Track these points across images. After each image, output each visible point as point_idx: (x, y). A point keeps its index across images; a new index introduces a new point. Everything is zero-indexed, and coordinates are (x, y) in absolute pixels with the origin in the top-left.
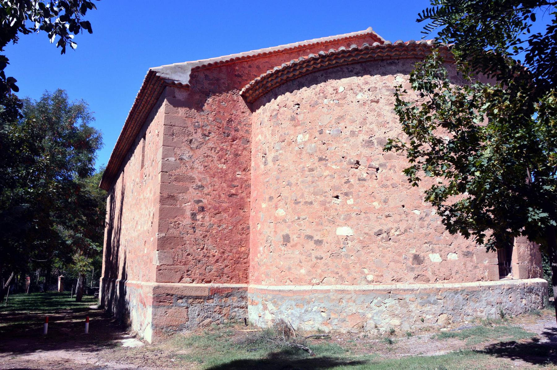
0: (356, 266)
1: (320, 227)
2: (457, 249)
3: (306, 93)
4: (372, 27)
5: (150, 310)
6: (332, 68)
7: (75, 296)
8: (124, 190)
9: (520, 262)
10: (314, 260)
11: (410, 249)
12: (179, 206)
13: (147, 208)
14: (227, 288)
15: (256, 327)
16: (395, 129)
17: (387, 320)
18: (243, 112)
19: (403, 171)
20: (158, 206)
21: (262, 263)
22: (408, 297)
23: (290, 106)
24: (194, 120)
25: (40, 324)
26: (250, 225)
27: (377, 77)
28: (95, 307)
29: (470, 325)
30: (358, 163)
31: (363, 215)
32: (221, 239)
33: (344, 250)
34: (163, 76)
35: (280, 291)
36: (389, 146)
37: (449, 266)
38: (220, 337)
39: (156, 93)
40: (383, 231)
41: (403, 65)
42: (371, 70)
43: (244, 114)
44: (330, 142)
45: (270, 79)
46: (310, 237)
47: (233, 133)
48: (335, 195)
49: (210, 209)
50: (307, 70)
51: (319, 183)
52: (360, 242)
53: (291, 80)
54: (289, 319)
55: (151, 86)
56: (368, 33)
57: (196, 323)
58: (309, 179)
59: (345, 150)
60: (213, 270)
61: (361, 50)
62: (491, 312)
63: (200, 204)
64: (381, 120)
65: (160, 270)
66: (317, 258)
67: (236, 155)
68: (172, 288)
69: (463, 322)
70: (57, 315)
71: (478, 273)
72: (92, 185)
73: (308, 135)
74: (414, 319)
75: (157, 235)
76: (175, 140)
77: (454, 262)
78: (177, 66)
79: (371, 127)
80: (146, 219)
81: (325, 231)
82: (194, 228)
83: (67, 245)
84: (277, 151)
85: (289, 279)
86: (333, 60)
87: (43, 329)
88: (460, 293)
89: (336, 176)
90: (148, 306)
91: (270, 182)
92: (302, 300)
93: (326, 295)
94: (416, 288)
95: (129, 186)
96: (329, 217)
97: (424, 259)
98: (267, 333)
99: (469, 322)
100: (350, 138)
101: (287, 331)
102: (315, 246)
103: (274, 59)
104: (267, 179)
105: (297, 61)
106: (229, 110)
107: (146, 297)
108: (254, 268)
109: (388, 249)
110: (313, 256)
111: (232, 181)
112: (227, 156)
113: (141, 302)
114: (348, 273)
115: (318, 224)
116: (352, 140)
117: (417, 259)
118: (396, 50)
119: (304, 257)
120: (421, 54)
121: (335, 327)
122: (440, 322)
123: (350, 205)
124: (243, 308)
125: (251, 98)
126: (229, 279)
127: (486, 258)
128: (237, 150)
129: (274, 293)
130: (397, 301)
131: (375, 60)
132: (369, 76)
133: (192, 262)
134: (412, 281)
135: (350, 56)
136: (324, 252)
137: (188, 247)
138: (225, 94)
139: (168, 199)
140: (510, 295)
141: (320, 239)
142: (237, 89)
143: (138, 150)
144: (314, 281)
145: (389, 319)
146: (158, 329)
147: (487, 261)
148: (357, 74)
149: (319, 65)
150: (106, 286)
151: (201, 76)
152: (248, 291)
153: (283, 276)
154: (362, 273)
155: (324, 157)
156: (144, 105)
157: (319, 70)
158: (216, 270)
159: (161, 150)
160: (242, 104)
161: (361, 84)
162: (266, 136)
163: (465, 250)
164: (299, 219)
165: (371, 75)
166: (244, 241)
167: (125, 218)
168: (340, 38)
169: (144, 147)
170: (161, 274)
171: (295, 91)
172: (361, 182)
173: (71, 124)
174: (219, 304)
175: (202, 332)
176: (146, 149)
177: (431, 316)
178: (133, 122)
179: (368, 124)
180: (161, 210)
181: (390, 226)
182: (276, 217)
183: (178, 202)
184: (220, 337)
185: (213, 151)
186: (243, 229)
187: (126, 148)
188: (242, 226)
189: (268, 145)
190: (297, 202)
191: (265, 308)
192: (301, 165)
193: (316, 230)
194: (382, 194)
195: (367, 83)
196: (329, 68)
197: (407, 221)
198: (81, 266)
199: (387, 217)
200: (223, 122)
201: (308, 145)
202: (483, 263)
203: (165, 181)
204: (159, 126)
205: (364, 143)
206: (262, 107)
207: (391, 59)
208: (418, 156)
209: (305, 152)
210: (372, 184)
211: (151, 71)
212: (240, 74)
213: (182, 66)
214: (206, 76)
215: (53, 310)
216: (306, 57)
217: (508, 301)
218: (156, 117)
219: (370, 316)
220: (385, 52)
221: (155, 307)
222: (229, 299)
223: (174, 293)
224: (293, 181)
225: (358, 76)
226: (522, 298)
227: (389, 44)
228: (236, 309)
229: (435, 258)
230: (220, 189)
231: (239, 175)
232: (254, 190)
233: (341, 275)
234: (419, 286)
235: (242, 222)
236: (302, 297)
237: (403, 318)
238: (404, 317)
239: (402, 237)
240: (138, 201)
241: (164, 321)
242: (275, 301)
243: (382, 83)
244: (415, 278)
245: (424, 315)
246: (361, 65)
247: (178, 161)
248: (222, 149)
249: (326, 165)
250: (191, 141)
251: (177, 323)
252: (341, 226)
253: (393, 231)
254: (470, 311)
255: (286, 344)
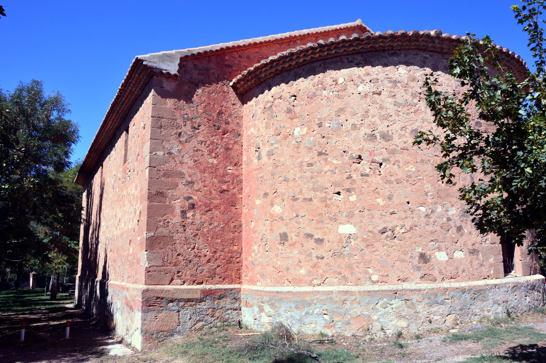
0: (359, 266)
1: (320, 225)
2: (463, 247)
3: (303, 85)
4: (362, 19)
5: (138, 315)
6: (332, 58)
7: (49, 293)
8: (104, 184)
9: (523, 258)
10: (315, 260)
11: (416, 247)
12: (168, 203)
13: (132, 205)
14: (219, 289)
15: (252, 331)
16: (398, 122)
17: (393, 322)
18: (234, 104)
19: (436, 167)
20: (146, 203)
21: (257, 263)
22: (415, 298)
23: (286, 98)
24: (182, 112)
25: (16, 328)
26: (243, 223)
27: (379, 68)
28: (71, 306)
29: (479, 326)
30: (360, 157)
31: (366, 212)
32: (212, 238)
33: (347, 248)
34: (150, 64)
35: (278, 292)
36: (420, 139)
37: (455, 264)
38: (216, 343)
39: (141, 83)
40: (388, 229)
41: (406, 56)
42: (372, 60)
43: (235, 107)
44: (330, 136)
45: (264, 69)
46: (310, 236)
47: (224, 126)
48: (337, 191)
49: (200, 206)
50: (304, 60)
51: (318, 179)
52: (364, 240)
53: (286, 70)
54: (289, 322)
55: (137, 75)
56: (358, 25)
57: (188, 327)
58: (308, 174)
59: (346, 144)
60: (205, 271)
61: (363, 40)
62: (497, 311)
63: (191, 201)
64: (383, 112)
65: (149, 272)
66: (318, 257)
67: (227, 149)
68: (162, 291)
69: (471, 322)
70: (32, 317)
71: (485, 271)
72: (68, 178)
73: (306, 129)
74: (422, 321)
75: (145, 235)
76: (163, 133)
77: (460, 261)
78: (165, 54)
79: (373, 120)
80: (131, 216)
81: (326, 229)
82: (184, 226)
83: (44, 243)
84: (272, 145)
85: (287, 279)
86: (333, 50)
87: (19, 334)
88: (468, 292)
89: (337, 171)
90: (135, 310)
91: (265, 178)
92: (302, 302)
93: (329, 296)
94: (423, 288)
95: (109, 182)
96: (330, 214)
97: (430, 258)
98: (265, 336)
99: (477, 322)
100: (352, 132)
101: (288, 336)
102: (316, 244)
103: (264, 50)
104: (262, 175)
105: (294, 50)
106: (220, 102)
107: (134, 301)
108: (247, 267)
109: (394, 247)
110: (314, 255)
111: (224, 176)
112: (218, 150)
113: (127, 305)
114: (352, 273)
115: (318, 222)
116: (354, 133)
117: (422, 256)
118: (399, 40)
119: (304, 257)
120: (424, 45)
121: (339, 331)
122: (448, 323)
123: (352, 202)
124: (236, 310)
125: (242, 89)
126: (221, 280)
127: (492, 256)
128: (228, 143)
129: (272, 294)
130: (404, 302)
131: (377, 51)
132: (370, 67)
133: (183, 263)
134: (418, 280)
135: (351, 45)
136: (326, 251)
137: (178, 246)
138: (214, 85)
139: (156, 196)
140: (515, 293)
141: (321, 238)
142: (228, 80)
143: (120, 144)
144: (315, 282)
145: (396, 321)
146: (148, 335)
147: (492, 259)
148: (358, 65)
149: (318, 55)
150: (84, 284)
151: (190, 65)
152: (242, 292)
153: (280, 277)
154: (367, 273)
155: (324, 152)
156: (128, 96)
157: (317, 60)
158: (208, 270)
159: (148, 144)
160: (233, 96)
161: (362, 76)
162: (259, 130)
163: (471, 247)
164: (297, 216)
165: (373, 66)
166: (236, 240)
167: (105, 215)
168: (330, 30)
169: (126, 141)
170: (149, 276)
171: (291, 82)
172: (363, 177)
173: (47, 117)
174: (212, 306)
175: (195, 337)
176: (129, 143)
177: (439, 317)
178: (115, 114)
179: (370, 116)
180: (149, 208)
181: (395, 223)
182: (272, 215)
183: (167, 199)
184: (216, 343)
185: (203, 145)
186: (235, 226)
187: (106, 142)
188: (234, 224)
189: (262, 138)
190: (295, 199)
191: (261, 310)
192: (299, 160)
193: (316, 229)
194: (386, 190)
195: (368, 74)
196: (327, 59)
197: (413, 218)
198: (56, 264)
199: (391, 214)
200: (213, 114)
201: (306, 139)
202: (488, 261)
203: (153, 176)
204: (146, 119)
205: (366, 136)
206: (254, 99)
207: (392, 49)
208: (452, 151)
209: (303, 146)
210: (375, 180)
211: (137, 59)
212: (230, 64)
213: (170, 54)
214: (195, 65)
215: (27, 310)
216: (304, 47)
217: (513, 299)
218: (141, 109)
219: (375, 317)
220: (387, 43)
221: (144, 311)
222: (221, 301)
223: (165, 296)
224: (290, 176)
225: (358, 67)
226: (526, 296)
227: (392, 34)
228: (229, 312)
229: (442, 256)
230: (211, 184)
231: (231, 169)
232: (247, 186)
233: (344, 276)
234: (426, 285)
235: (234, 219)
236: (302, 299)
237: (410, 319)
238: (411, 318)
239: (407, 235)
240: (121, 197)
241: (154, 326)
242: (272, 303)
243: (384, 74)
244: (422, 277)
245: (432, 316)
246: (362, 56)
247: (167, 156)
248: (212, 143)
249: (326, 160)
250: (180, 133)
251: (168, 328)
252: (343, 224)
253: (398, 229)
254: (477, 311)
255: (289, 350)
